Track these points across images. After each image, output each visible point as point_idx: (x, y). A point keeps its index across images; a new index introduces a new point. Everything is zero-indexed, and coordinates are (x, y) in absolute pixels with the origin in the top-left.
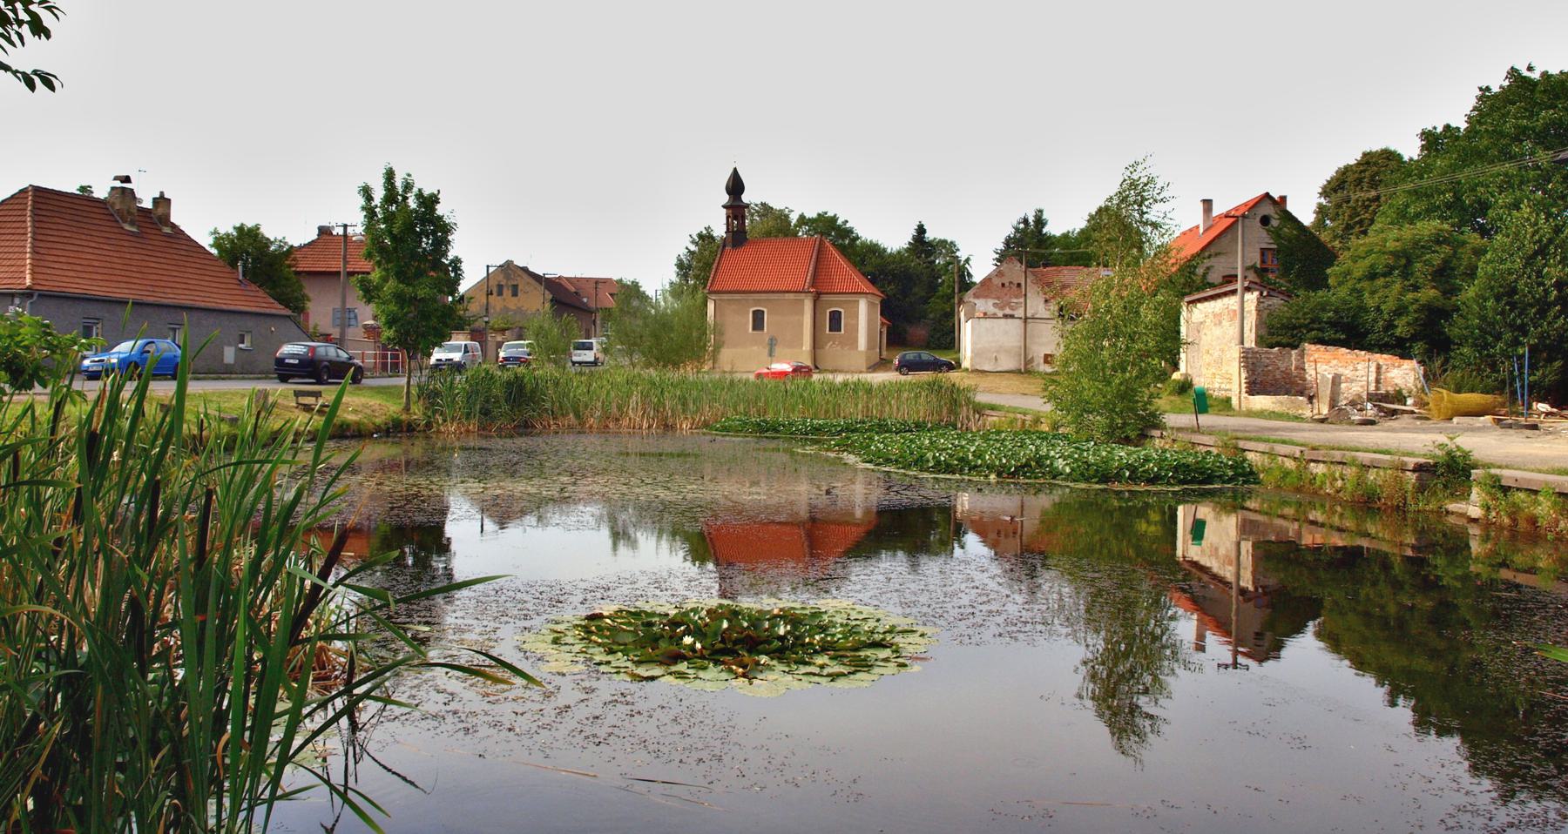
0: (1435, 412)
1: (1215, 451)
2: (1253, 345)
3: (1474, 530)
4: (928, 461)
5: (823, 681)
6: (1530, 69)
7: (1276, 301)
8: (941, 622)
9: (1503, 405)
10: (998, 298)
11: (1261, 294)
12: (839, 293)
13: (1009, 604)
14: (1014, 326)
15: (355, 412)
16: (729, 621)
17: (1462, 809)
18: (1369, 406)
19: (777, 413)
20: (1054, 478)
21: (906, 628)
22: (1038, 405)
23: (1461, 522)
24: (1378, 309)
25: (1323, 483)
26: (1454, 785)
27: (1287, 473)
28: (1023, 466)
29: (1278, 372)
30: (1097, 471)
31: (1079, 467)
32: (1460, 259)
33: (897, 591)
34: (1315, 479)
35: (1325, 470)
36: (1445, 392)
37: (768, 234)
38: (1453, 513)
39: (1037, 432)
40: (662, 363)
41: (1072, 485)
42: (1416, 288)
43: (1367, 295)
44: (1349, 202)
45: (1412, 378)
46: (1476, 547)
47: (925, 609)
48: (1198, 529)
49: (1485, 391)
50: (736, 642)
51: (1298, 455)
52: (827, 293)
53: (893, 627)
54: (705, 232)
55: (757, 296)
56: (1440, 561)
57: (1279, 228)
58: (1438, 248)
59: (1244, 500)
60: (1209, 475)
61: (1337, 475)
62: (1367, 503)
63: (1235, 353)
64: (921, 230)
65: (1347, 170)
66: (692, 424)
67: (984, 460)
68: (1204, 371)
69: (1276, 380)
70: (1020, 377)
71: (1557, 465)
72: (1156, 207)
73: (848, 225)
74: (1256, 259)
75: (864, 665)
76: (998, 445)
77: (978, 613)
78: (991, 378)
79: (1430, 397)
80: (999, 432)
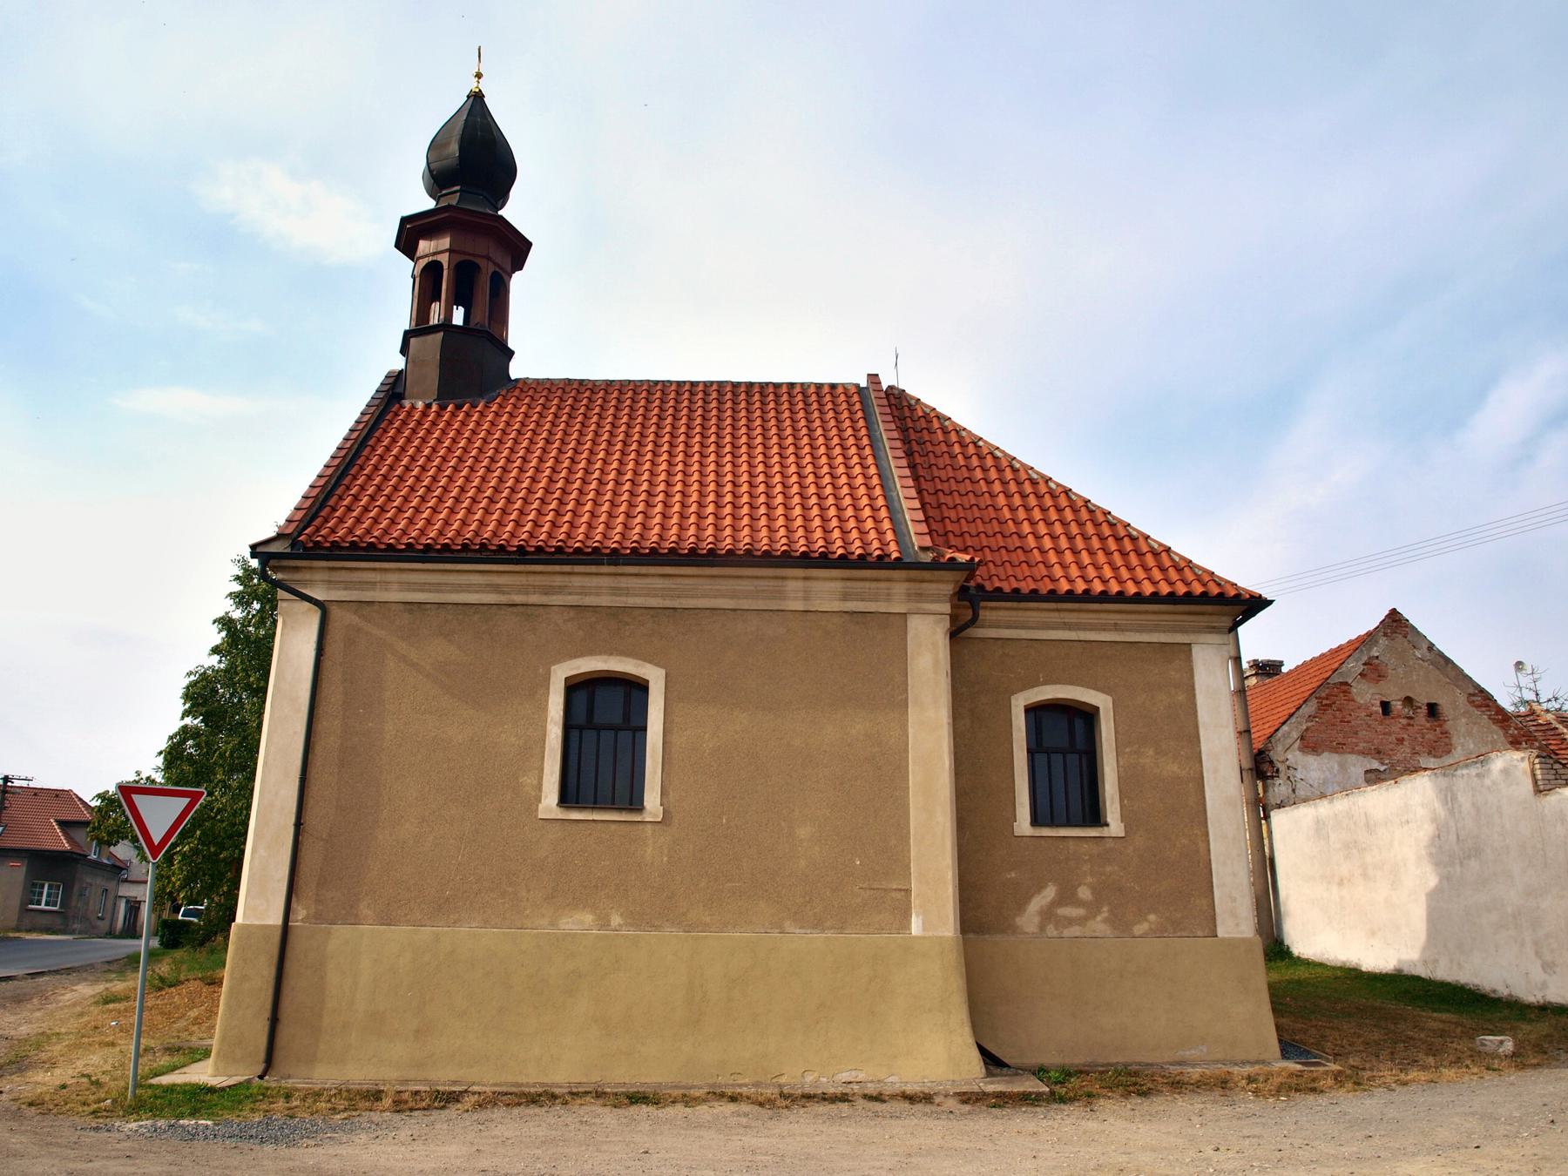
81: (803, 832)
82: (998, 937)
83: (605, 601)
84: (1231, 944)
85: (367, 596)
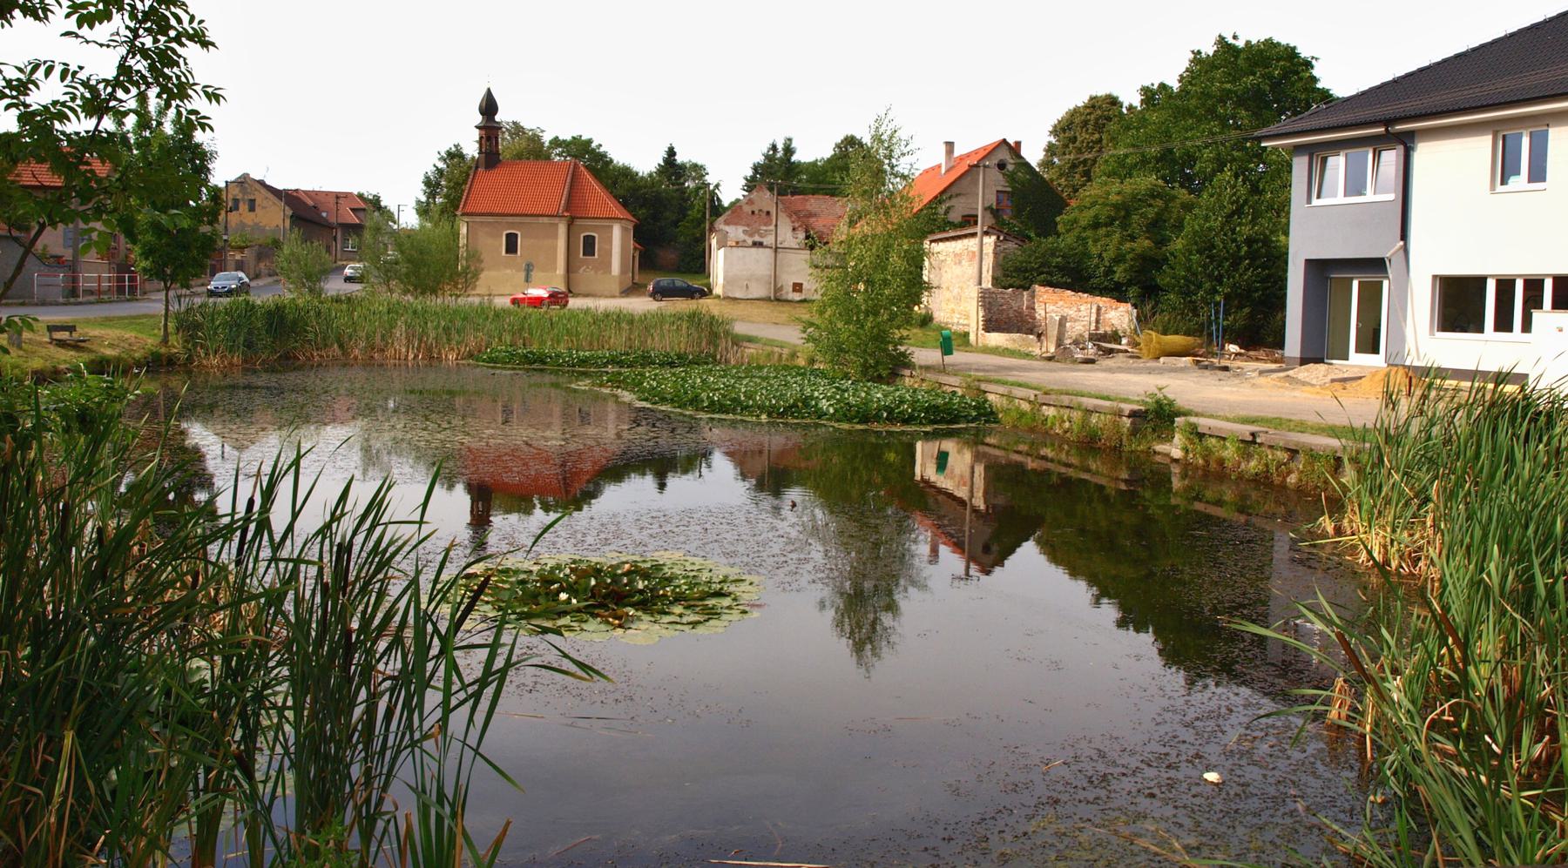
0: (1144, 351)
1: (960, 393)
2: (990, 286)
3: (1176, 469)
4: (703, 401)
5: (687, 628)
6: (1235, 37)
7: (1011, 246)
8: (762, 571)
9: (1201, 346)
10: (748, 225)
11: (998, 238)
12: (593, 218)
13: (813, 552)
14: (765, 255)
15: (111, 346)
16: (596, 578)
17: (1166, 710)
18: (1090, 345)
19: (543, 343)
20: (819, 418)
21: (736, 577)
22: (791, 336)
23: (1167, 461)
24: (1100, 256)
25: (1053, 424)
26: (1161, 693)
27: (1023, 414)
28: (791, 407)
29: (1011, 311)
30: (858, 412)
31: (842, 408)
32: (1171, 212)
33: (716, 541)
34: (1046, 420)
35: (1055, 413)
36: (1154, 334)
37: (519, 156)
38: (1159, 453)
39: (795, 367)
40: (419, 291)
41: (836, 425)
42: (1133, 238)
43: (1090, 242)
44: (1074, 143)
45: (1127, 320)
46: (1177, 483)
47: (745, 559)
48: (942, 461)
49: (1187, 334)
50: (605, 597)
51: (1032, 398)
52: (581, 218)
53: (726, 577)
54: (454, 149)
55: (510, 219)
56: (1148, 494)
57: (1013, 173)
58: (1152, 202)
59: (984, 436)
60: (955, 416)
61: (1065, 418)
62: (1089, 443)
63: (973, 292)
64: (671, 152)
65: (1075, 112)
66: (458, 355)
67: (754, 400)
68: (944, 306)
69: (1010, 318)
70: (770, 305)
71: (1243, 413)
72: (902, 160)
73: (602, 150)
74: (992, 200)
75: (712, 613)
76: (765, 384)
77: (790, 562)
78: (742, 305)
79: (1142, 338)
80: (760, 368)
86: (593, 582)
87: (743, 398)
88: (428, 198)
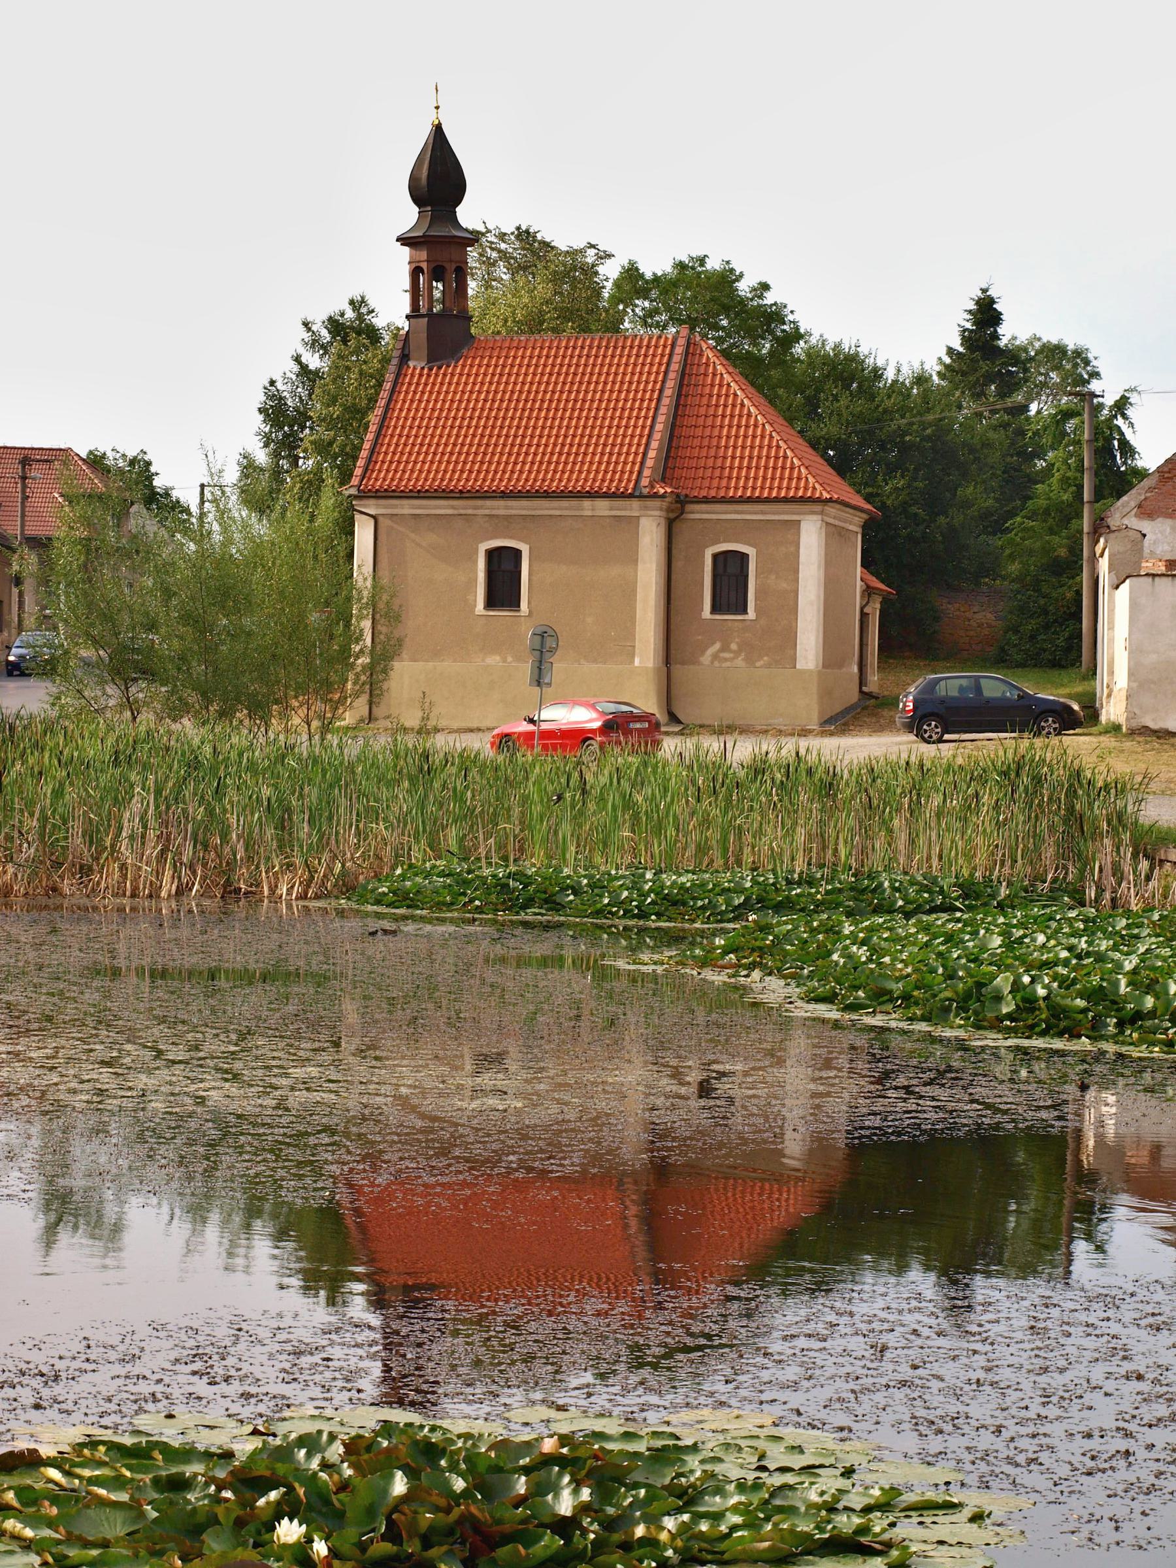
8: (1032, 1478)
12: (750, 500)
16: (412, 1473)
19: (556, 851)
21: (931, 1495)
33: (903, 1383)
47: (986, 1440)
52: (706, 500)
54: (350, 314)
55: (500, 507)
73: (770, 298)
77: (1141, 1454)
81: (589, 620)
82: (691, 667)
83: (502, 512)
84: (803, 672)
85: (395, 511)
86: (399, 1485)
87: (1123, 988)
88: (276, 455)
